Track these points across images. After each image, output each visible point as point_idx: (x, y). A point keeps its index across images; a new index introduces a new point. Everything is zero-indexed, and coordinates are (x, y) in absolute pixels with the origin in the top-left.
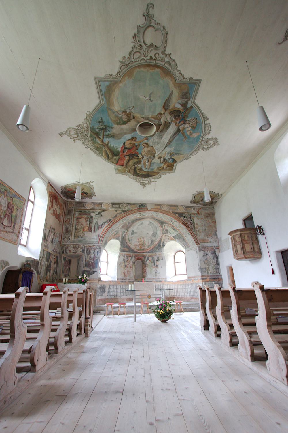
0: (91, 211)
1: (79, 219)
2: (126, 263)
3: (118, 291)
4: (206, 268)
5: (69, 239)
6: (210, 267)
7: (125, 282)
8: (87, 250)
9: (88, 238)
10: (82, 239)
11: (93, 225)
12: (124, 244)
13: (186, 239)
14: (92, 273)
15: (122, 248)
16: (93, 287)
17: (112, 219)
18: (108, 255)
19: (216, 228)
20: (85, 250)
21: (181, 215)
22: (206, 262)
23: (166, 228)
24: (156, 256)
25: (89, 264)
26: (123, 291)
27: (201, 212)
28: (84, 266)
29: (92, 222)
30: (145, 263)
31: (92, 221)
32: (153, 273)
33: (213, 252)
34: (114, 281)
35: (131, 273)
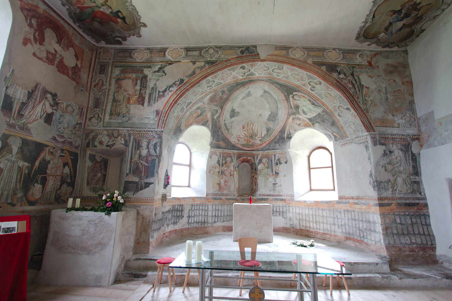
0: (145, 64)
1: (121, 80)
3: (207, 215)
4: (389, 181)
5: (100, 120)
6: (400, 180)
7: (221, 199)
8: (135, 139)
9: (137, 116)
10: (125, 119)
11: (148, 92)
12: (218, 135)
13: (341, 121)
14: (143, 186)
15: (214, 142)
16: (144, 215)
17: (186, 80)
19: (412, 95)
20: (130, 142)
21: (332, 68)
22: (389, 167)
24: (275, 156)
25: (137, 168)
26: (217, 215)
27: (377, 62)
28: (128, 172)
29: (146, 87)
30: (255, 169)
31: (146, 85)
32: (270, 185)
33: (406, 148)
34: (201, 198)
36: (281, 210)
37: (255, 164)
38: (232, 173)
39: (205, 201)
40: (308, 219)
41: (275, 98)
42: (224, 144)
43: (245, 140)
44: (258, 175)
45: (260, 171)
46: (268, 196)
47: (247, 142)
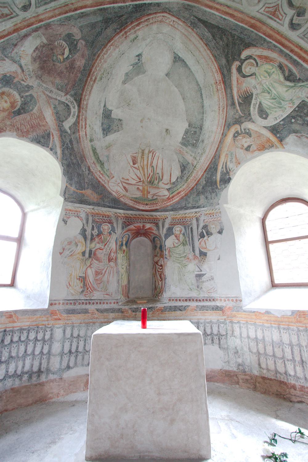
2: (93, 245)
3: (49, 352)
7: (86, 311)
12: (79, 175)
15: (73, 188)
18: (24, 215)
24: (197, 220)
26: (73, 350)
30: (161, 247)
32: (191, 278)
34: (34, 312)
35: (111, 279)
36: (215, 331)
37: (160, 237)
38: (112, 254)
39: (45, 319)
40: (279, 354)
41: (198, 80)
42: (96, 195)
43: (138, 188)
44: (165, 260)
45: (169, 251)
46: (186, 300)
47: (144, 195)
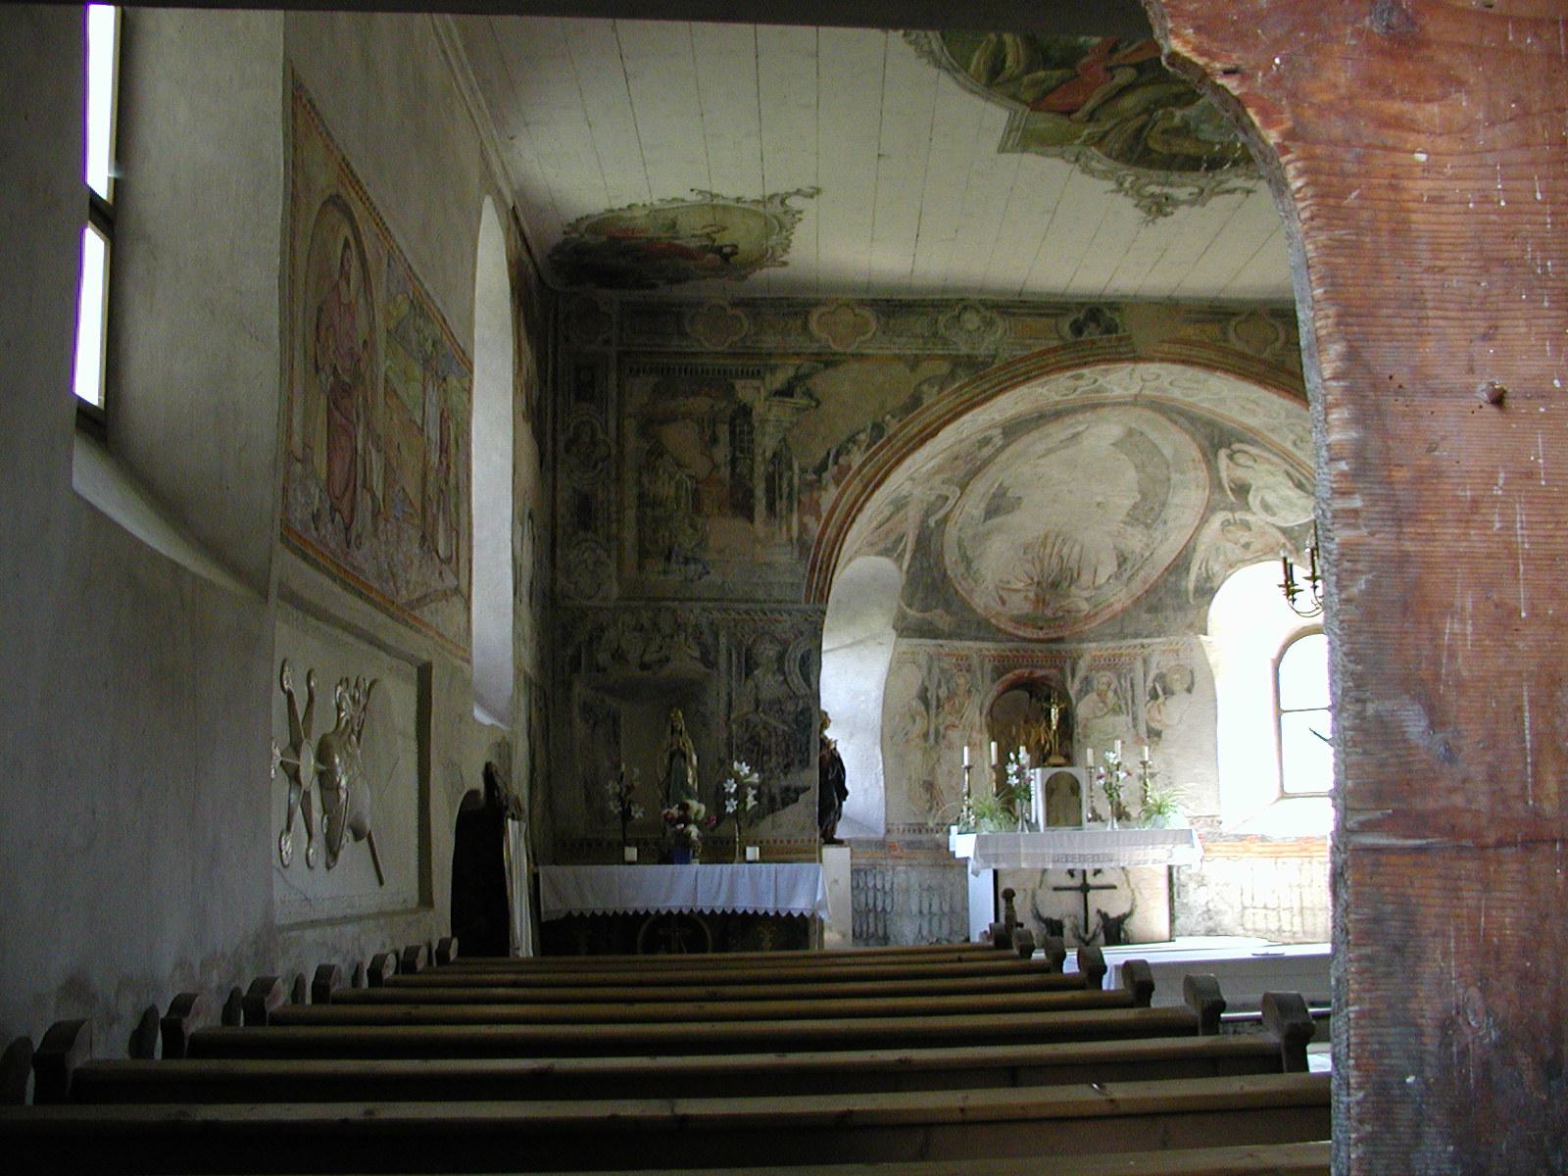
14: (778, 798)
23: (1240, 473)
24: (1145, 661)
